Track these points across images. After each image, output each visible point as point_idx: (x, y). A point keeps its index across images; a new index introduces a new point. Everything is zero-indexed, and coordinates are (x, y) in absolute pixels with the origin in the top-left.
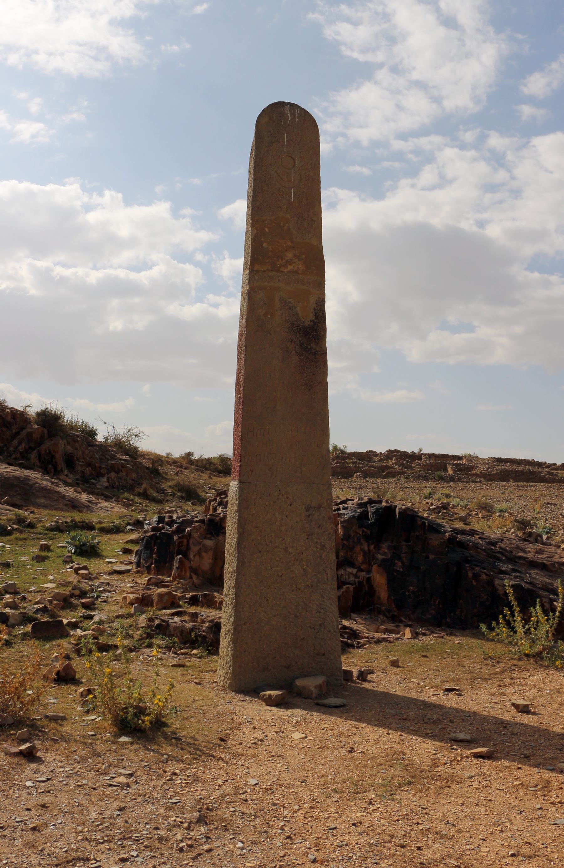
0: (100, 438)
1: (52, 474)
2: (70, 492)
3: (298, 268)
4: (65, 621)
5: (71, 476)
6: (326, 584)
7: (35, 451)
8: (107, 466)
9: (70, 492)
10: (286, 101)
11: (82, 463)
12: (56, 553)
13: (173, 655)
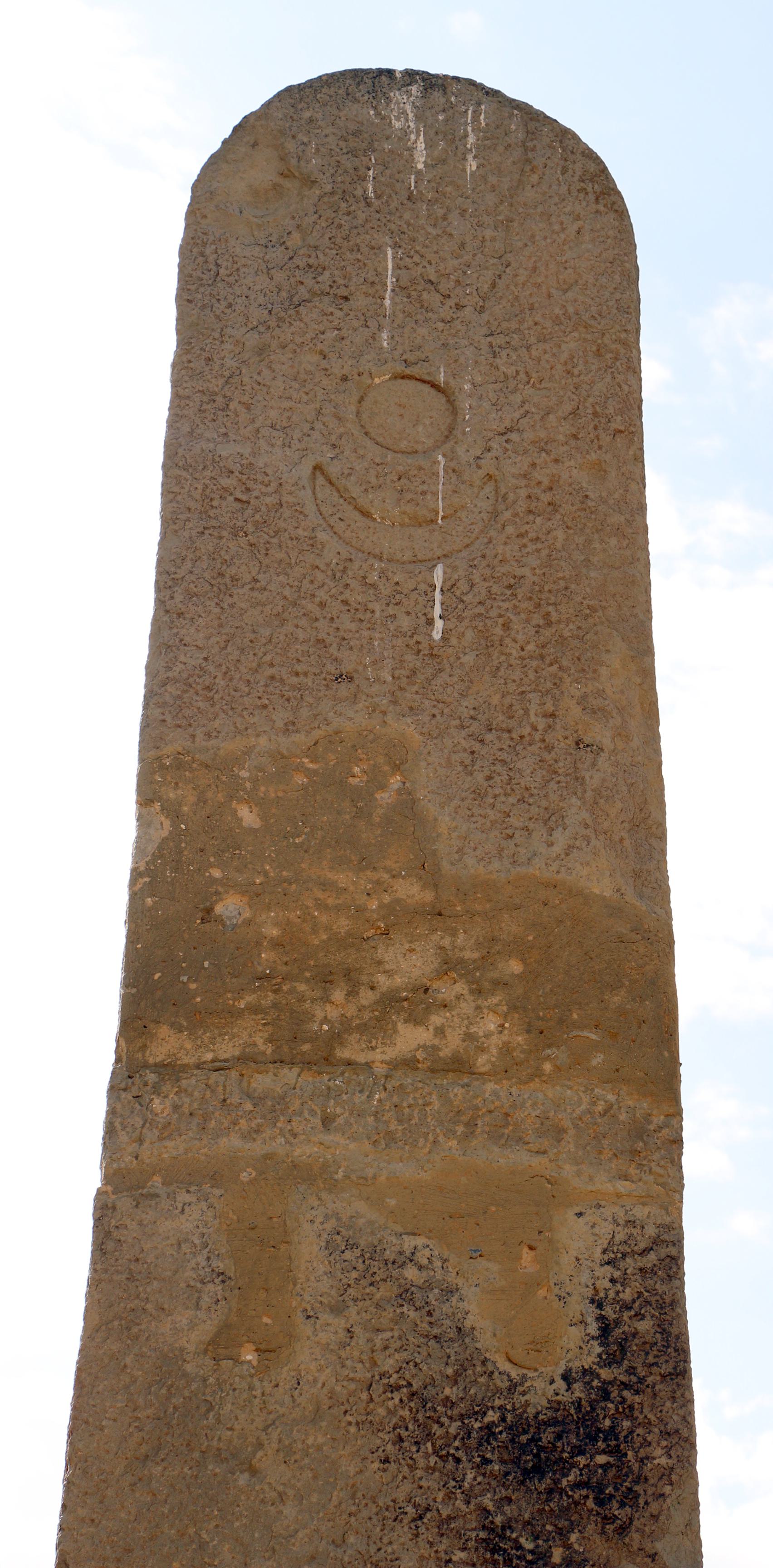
3: (469, 1037)
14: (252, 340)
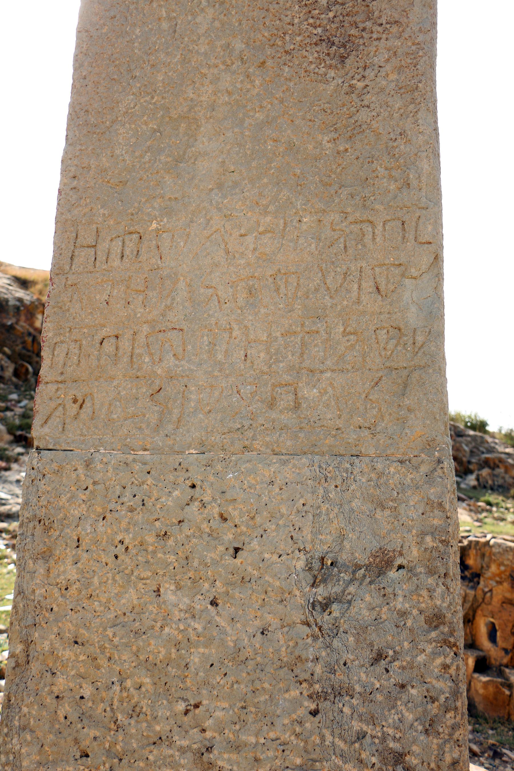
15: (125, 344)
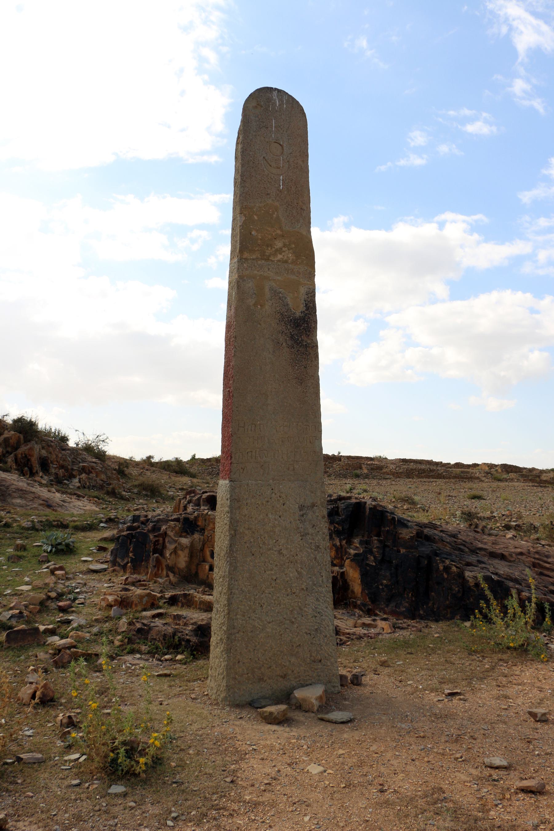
0: (71, 444)
1: (28, 476)
2: (44, 492)
3: (287, 257)
4: (42, 628)
5: (46, 477)
6: (320, 586)
7: (12, 455)
8: (79, 468)
9: (44, 492)
10: (274, 86)
11: (56, 466)
12: (32, 553)
13: (157, 662)
14: (254, 134)
15: (254, 454)
